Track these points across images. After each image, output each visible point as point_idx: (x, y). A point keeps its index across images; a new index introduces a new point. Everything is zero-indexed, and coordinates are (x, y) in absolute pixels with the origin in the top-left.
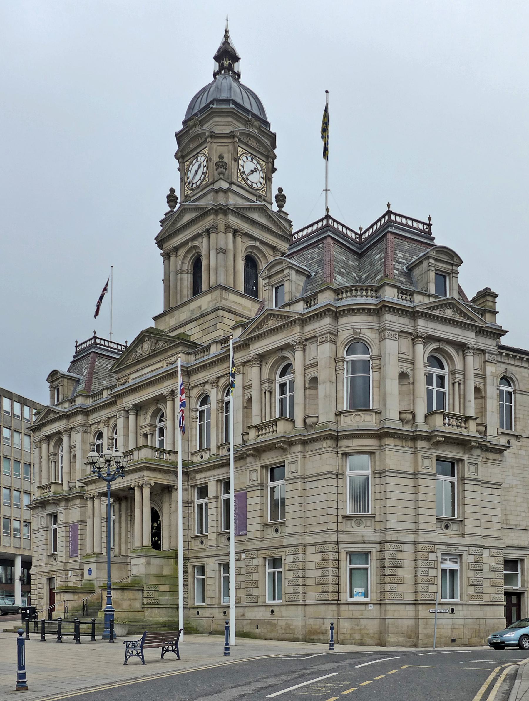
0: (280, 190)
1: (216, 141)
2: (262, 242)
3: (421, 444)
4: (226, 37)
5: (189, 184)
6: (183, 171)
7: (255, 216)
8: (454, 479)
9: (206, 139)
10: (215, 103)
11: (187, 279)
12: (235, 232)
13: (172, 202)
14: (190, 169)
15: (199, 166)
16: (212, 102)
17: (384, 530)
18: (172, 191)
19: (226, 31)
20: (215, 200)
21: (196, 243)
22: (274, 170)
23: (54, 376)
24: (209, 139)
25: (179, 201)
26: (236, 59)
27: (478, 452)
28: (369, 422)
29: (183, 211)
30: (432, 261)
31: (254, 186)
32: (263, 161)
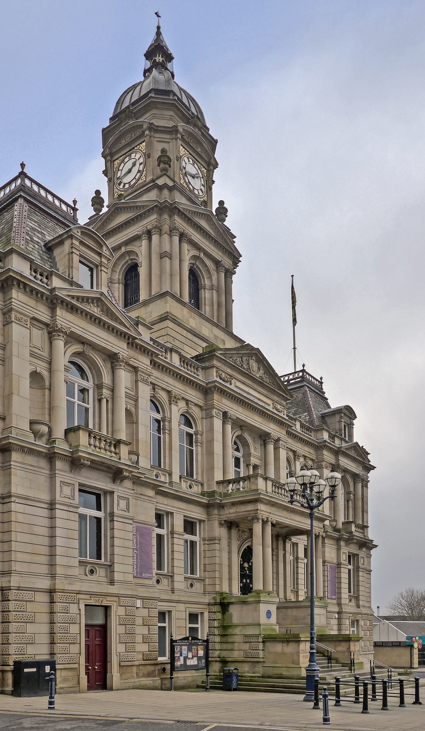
0: (221, 203)
1: (157, 135)
4: (158, 33)
5: (120, 184)
8: (351, 567)
9: (143, 132)
10: (153, 92)
12: (182, 236)
13: (98, 204)
14: (121, 168)
15: (134, 164)
16: (150, 92)
18: (98, 192)
19: (158, 28)
20: (159, 196)
21: (130, 248)
23: (234, 242)
24: (147, 132)
25: (106, 203)
26: (169, 58)
29: (115, 210)
30: (343, 415)
31: (196, 192)
32: (204, 167)
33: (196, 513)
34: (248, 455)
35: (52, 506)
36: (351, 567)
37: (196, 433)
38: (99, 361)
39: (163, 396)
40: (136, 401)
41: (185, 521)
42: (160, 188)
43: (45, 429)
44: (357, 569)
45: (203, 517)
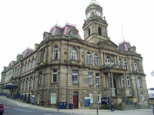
0: (104, 16)
2: (101, 25)
3: (68, 67)
6: (87, 16)
7: (100, 21)
8: (140, 80)
11: (88, 34)
17: (59, 86)
21: (89, 27)
22: (102, 13)
27: (82, 68)
28: (57, 62)
33: (98, 72)
34: (110, 59)
35: (67, 74)
36: (140, 80)
37: (91, 55)
38: (77, 48)
39: (121, 58)
40: (84, 53)
41: (96, 74)
42: (92, 17)
43: (84, 63)
44: (141, 80)
45: (100, 73)
